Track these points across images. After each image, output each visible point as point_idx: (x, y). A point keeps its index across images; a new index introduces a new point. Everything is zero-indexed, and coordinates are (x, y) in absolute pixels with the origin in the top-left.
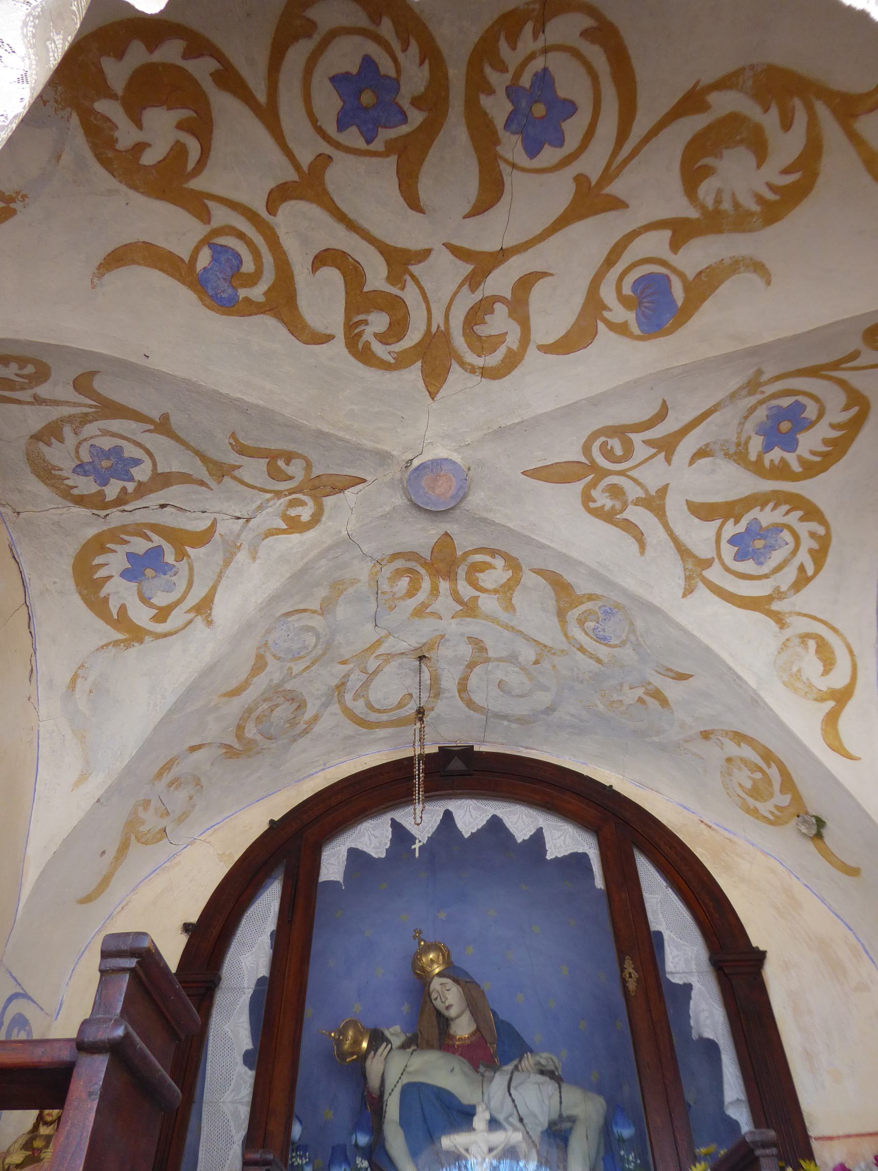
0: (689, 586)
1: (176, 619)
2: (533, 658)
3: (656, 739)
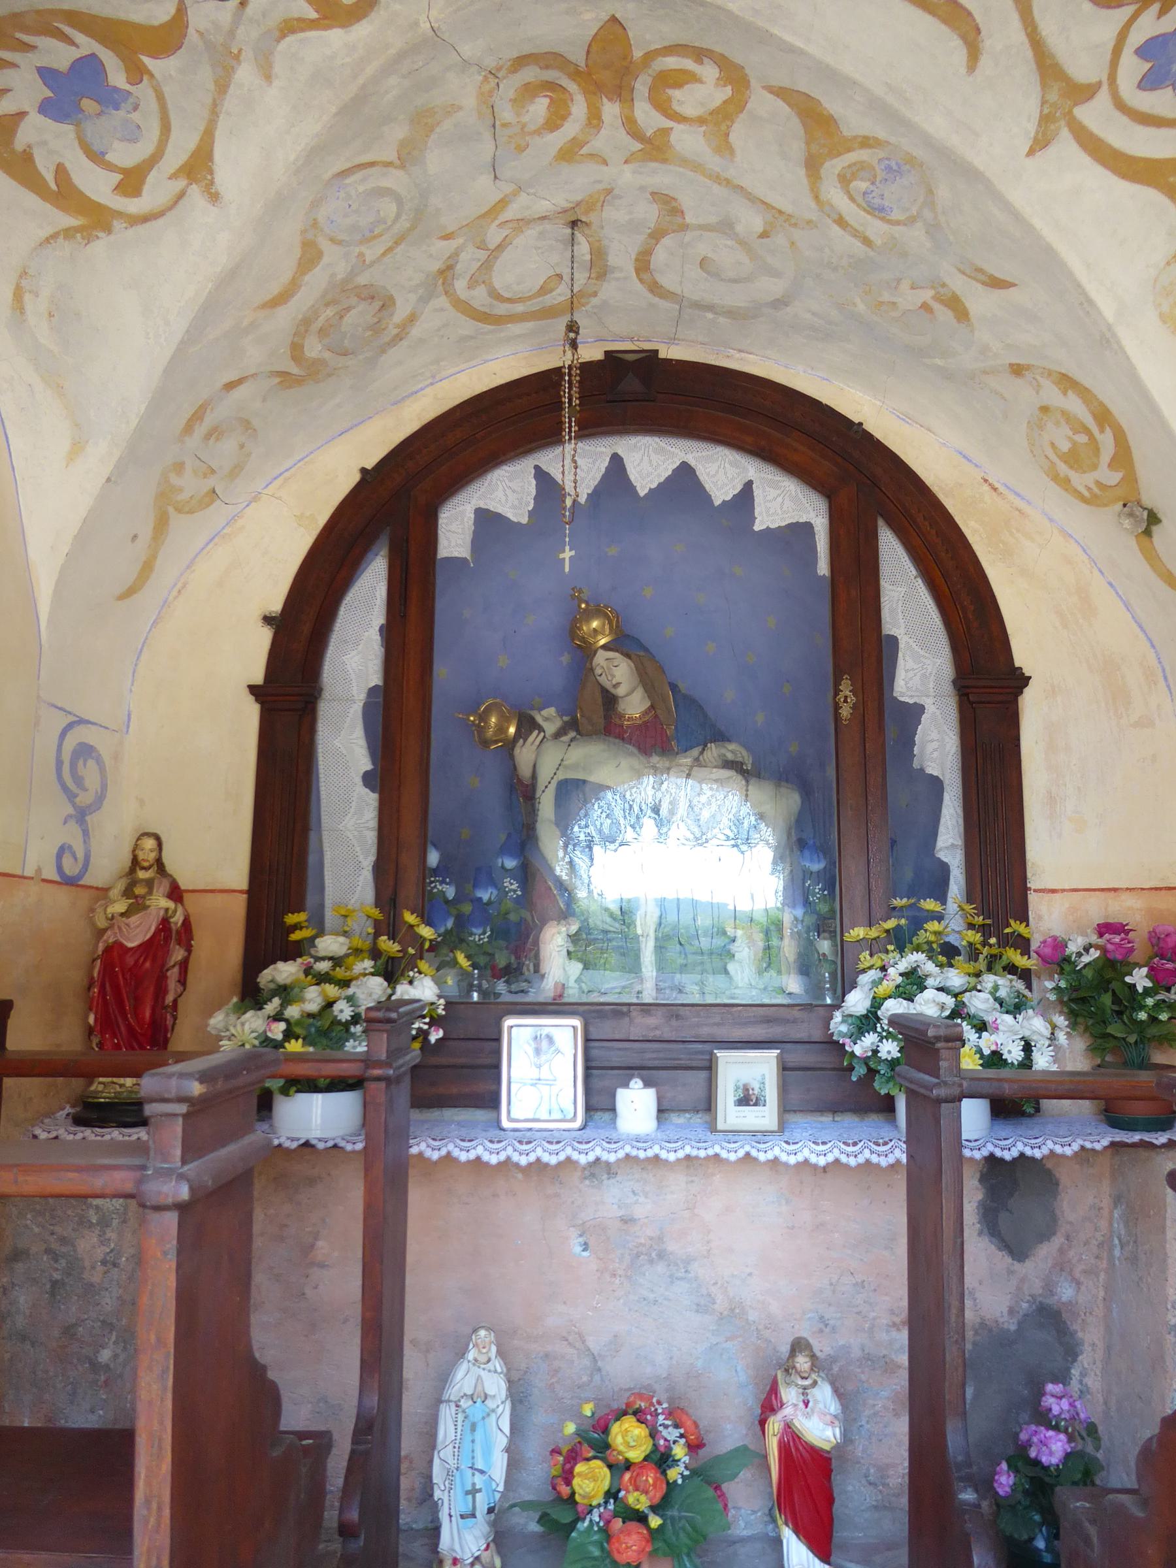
0: (1044, 134)
1: (158, 189)
2: (760, 229)
3: (938, 362)
